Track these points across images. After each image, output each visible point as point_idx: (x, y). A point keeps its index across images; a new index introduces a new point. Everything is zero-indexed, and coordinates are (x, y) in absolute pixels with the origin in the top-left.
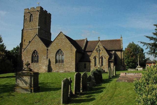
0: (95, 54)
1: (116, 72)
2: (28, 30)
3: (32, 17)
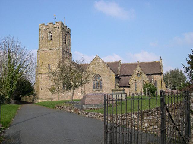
0: (134, 77)
1: (159, 61)
2: (46, 51)
3: (50, 35)
